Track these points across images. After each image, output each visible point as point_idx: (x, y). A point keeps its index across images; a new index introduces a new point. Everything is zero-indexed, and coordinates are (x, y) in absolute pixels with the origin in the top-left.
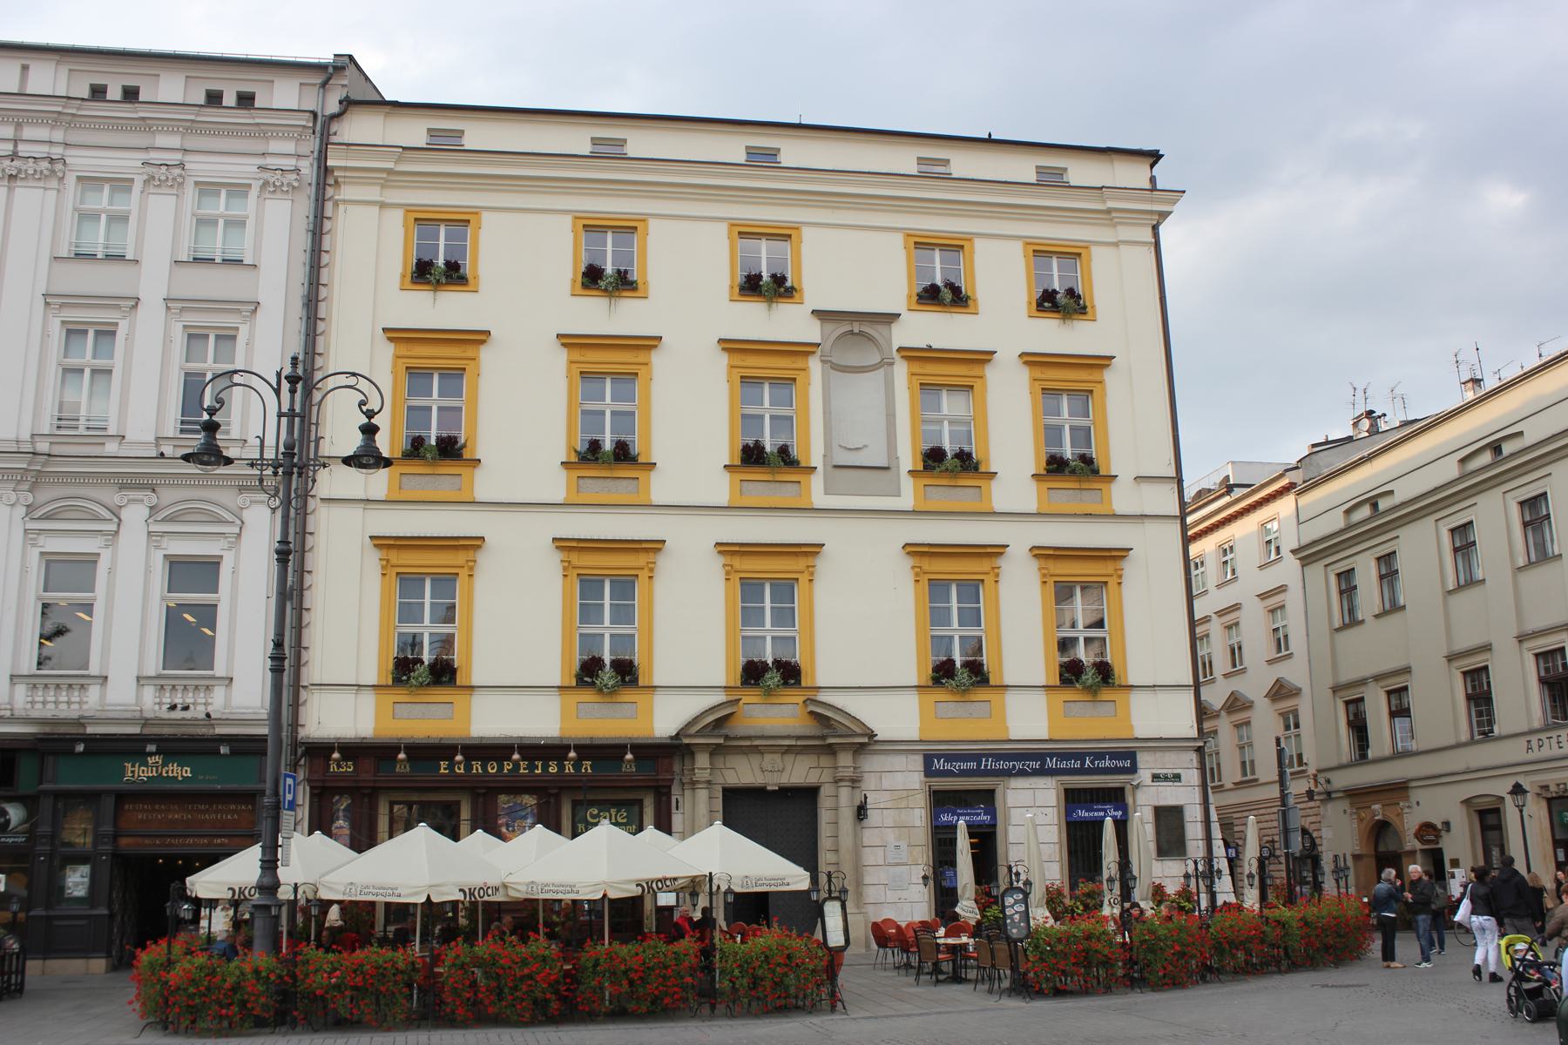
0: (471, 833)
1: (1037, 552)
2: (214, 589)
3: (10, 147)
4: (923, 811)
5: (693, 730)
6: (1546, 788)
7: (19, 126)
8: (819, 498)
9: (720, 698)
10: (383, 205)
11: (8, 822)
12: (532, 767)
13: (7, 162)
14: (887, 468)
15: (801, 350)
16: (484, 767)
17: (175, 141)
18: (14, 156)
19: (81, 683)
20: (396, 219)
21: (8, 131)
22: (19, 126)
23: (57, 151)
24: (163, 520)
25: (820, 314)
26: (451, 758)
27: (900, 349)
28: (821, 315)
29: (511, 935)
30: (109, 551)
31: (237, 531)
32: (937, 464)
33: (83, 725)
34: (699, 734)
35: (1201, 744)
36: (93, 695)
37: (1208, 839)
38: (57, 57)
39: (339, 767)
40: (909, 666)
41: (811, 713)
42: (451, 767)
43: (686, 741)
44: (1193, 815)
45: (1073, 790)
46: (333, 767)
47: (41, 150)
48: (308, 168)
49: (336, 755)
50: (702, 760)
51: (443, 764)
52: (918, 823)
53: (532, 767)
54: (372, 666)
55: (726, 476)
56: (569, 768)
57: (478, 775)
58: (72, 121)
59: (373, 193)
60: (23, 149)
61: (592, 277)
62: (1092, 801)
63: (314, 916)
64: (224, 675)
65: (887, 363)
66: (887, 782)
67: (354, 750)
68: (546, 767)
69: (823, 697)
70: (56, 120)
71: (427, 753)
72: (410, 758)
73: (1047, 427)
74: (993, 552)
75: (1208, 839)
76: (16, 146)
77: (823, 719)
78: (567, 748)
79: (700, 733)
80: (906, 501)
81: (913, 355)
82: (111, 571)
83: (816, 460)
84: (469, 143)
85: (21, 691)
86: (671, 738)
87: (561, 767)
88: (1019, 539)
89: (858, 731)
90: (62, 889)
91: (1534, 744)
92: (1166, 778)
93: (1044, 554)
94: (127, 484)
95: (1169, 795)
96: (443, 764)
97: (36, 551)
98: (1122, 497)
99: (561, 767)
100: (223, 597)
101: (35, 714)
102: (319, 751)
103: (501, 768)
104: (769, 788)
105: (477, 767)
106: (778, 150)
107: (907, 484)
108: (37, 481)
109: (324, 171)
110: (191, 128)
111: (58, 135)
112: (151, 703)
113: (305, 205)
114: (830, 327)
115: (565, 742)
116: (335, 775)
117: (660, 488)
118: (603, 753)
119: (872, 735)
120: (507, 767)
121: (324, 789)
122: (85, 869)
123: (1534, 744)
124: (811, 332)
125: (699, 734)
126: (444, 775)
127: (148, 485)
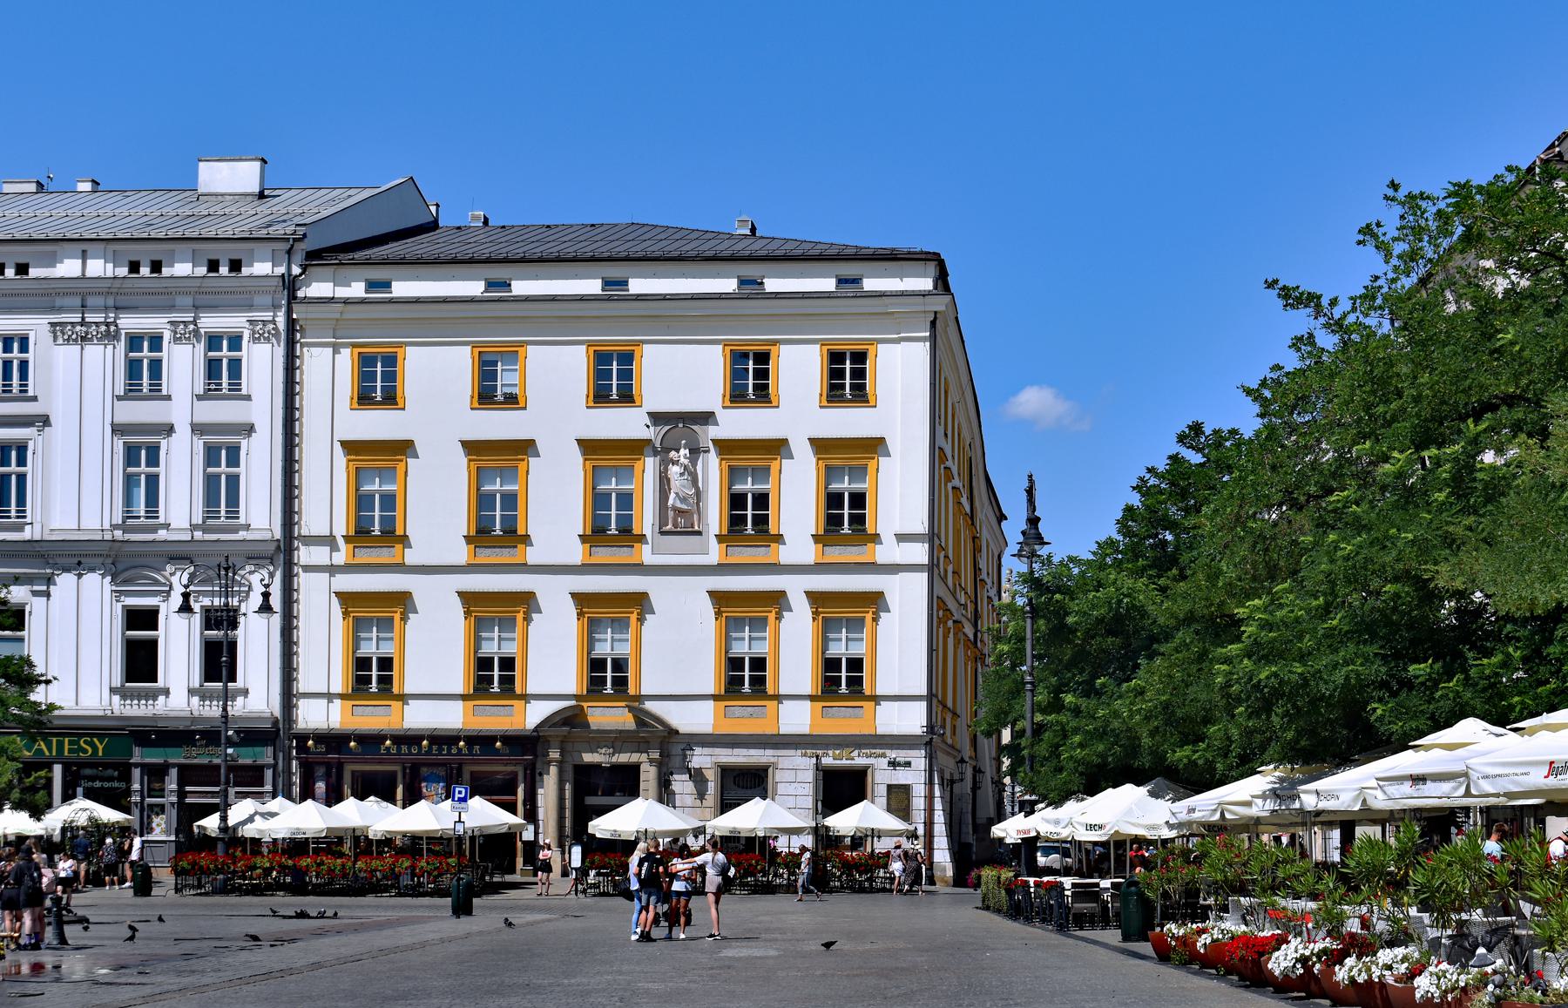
0: (722, 813)
2: (155, 628)
8: (647, 555)
15: (636, 448)
19: (153, 695)
28: (657, 418)
32: (108, 537)
33: (156, 721)
37: (930, 810)
40: (708, 678)
44: (919, 791)
63: (576, 869)
69: (650, 706)
71: (371, 741)
75: (930, 810)
77: (643, 718)
78: (422, 738)
80: (340, 558)
81: (726, 447)
83: (647, 531)
85: (195, 700)
88: (796, 587)
95: (901, 777)
97: (120, 605)
98: (887, 552)
102: (302, 738)
109: (291, 324)
112: (451, 717)
118: (481, 741)
126: (383, 754)
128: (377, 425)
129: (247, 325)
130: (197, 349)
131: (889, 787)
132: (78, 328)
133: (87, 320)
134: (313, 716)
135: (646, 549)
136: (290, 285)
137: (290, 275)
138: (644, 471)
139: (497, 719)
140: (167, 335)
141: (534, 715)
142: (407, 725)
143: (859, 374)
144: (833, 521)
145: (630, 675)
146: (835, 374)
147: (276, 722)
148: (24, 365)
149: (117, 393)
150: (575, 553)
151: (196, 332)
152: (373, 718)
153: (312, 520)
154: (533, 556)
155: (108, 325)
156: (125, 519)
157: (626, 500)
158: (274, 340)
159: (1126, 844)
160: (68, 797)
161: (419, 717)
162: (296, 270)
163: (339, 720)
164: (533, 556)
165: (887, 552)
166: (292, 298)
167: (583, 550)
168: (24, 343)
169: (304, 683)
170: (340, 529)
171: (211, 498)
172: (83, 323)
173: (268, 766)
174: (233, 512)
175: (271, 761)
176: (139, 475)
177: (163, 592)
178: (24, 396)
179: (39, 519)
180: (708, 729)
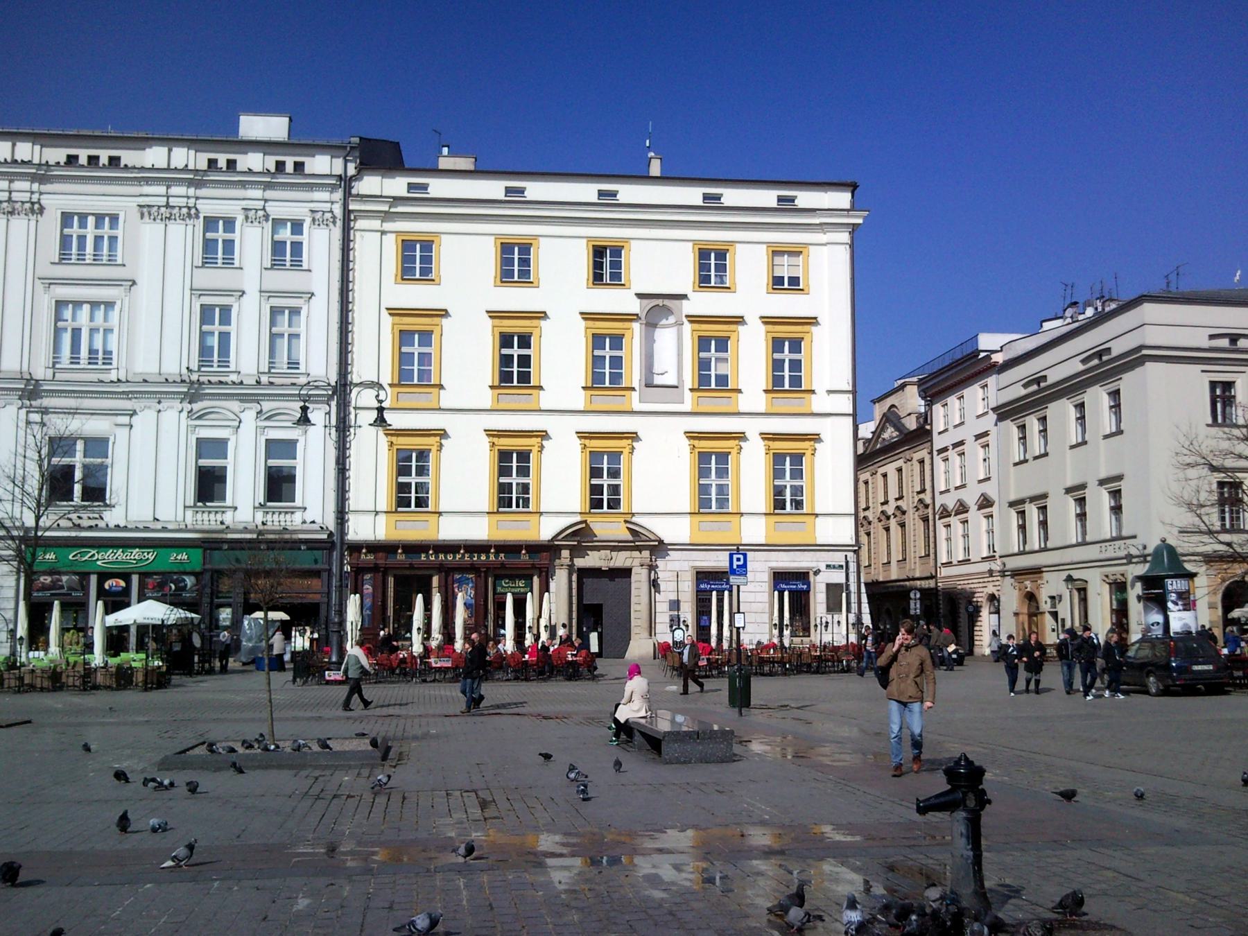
1: (688, 435)
3: (5, 196)
4: (690, 583)
5: (560, 537)
6: (1107, 576)
7: (168, 187)
9: (578, 518)
10: (383, 233)
11: (186, 585)
12: (471, 557)
13: (5, 205)
14: (677, 387)
16: (446, 557)
17: (258, 193)
18: (10, 200)
20: (390, 241)
21: (4, 184)
22: (168, 187)
23: (192, 202)
24: (266, 419)
25: (640, 296)
26: (427, 552)
27: (687, 316)
29: (708, 660)
30: (304, 437)
31: (237, 424)
34: (564, 539)
35: (856, 548)
36: (298, 517)
38: (188, 144)
39: (367, 558)
40: (684, 499)
41: (627, 528)
42: (427, 557)
43: (556, 543)
45: (778, 573)
46: (363, 556)
47: (182, 202)
48: (338, 210)
49: (364, 551)
50: (565, 553)
51: (423, 555)
52: (687, 589)
53: (471, 557)
54: (385, 499)
55: (490, 391)
56: (492, 557)
57: (442, 560)
58: (198, 184)
59: (376, 224)
60: (173, 201)
61: (777, 282)
62: (789, 580)
64: (231, 505)
65: (679, 324)
66: (671, 566)
67: (375, 547)
68: (479, 557)
69: (634, 519)
70: (190, 183)
72: (404, 552)
73: (774, 361)
74: (741, 437)
76: (168, 203)
78: (490, 547)
79: (565, 538)
80: (687, 406)
82: (114, 443)
84: (622, 198)
86: (549, 541)
87: (488, 557)
89: (653, 538)
90: (217, 620)
91: (1104, 549)
92: (834, 567)
93: (768, 437)
94: (244, 398)
96: (423, 555)
98: (819, 402)
99: (488, 557)
100: (298, 463)
101: (198, 527)
102: (356, 548)
103: (454, 557)
104: (603, 569)
105: (441, 556)
106: (428, 185)
107: (688, 396)
108: (192, 398)
109: (347, 213)
110: (268, 186)
111: (191, 191)
112: (478, 530)
113: (337, 232)
114: (645, 302)
115: (490, 543)
116: (364, 560)
117: (546, 399)
119: (661, 542)
120: (458, 556)
121: (358, 568)
122: (229, 610)
123: (1104, 549)
124: (634, 306)
125: (564, 539)
127: (256, 399)
128: (416, 295)
129: (309, 214)
130: (265, 230)
131: (828, 585)
132: (163, 209)
133: (171, 204)
134: (362, 529)
135: (635, 395)
136: (345, 183)
137: (346, 176)
138: (441, 335)
139: (514, 529)
140: (240, 219)
141: (547, 530)
142: (541, 539)
143: (525, 262)
144: (777, 381)
145: (623, 497)
146: (598, 266)
147: (331, 535)
148: (113, 239)
149: (195, 264)
150: (579, 400)
151: (267, 217)
152: (413, 529)
153: (362, 370)
154: (446, 399)
155: (189, 208)
156: (270, 368)
157: (617, 362)
158: (331, 225)
159: (116, 601)
160: (141, 599)
161: (451, 530)
162: (351, 170)
163: (384, 533)
164: (446, 399)
165: (819, 402)
166: (348, 194)
167: (766, 399)
168: (114, 219)
169: (353, 503)
170: (386, 379)
171: (205, 351)
172: (167, 206)
173: (325, 570)
174: (224, 362)
175: (327, 567)
176: (212, 333)
177: (233, 427)
178: (112, 262)
179: (124, 365)
180: (762, 540)
